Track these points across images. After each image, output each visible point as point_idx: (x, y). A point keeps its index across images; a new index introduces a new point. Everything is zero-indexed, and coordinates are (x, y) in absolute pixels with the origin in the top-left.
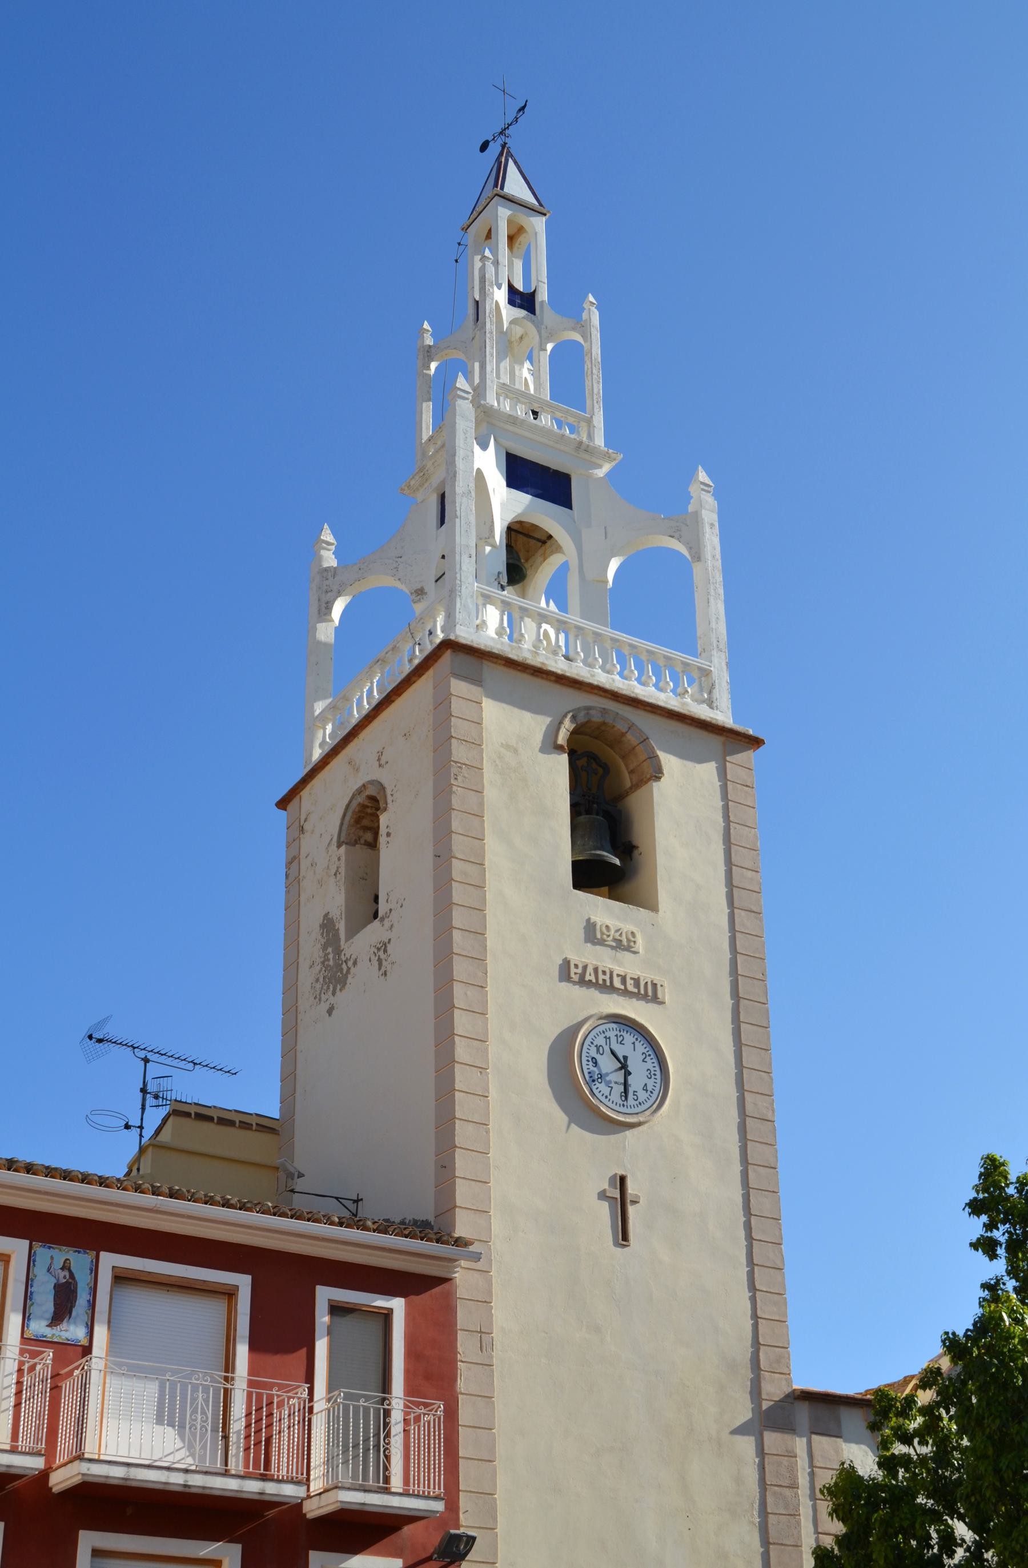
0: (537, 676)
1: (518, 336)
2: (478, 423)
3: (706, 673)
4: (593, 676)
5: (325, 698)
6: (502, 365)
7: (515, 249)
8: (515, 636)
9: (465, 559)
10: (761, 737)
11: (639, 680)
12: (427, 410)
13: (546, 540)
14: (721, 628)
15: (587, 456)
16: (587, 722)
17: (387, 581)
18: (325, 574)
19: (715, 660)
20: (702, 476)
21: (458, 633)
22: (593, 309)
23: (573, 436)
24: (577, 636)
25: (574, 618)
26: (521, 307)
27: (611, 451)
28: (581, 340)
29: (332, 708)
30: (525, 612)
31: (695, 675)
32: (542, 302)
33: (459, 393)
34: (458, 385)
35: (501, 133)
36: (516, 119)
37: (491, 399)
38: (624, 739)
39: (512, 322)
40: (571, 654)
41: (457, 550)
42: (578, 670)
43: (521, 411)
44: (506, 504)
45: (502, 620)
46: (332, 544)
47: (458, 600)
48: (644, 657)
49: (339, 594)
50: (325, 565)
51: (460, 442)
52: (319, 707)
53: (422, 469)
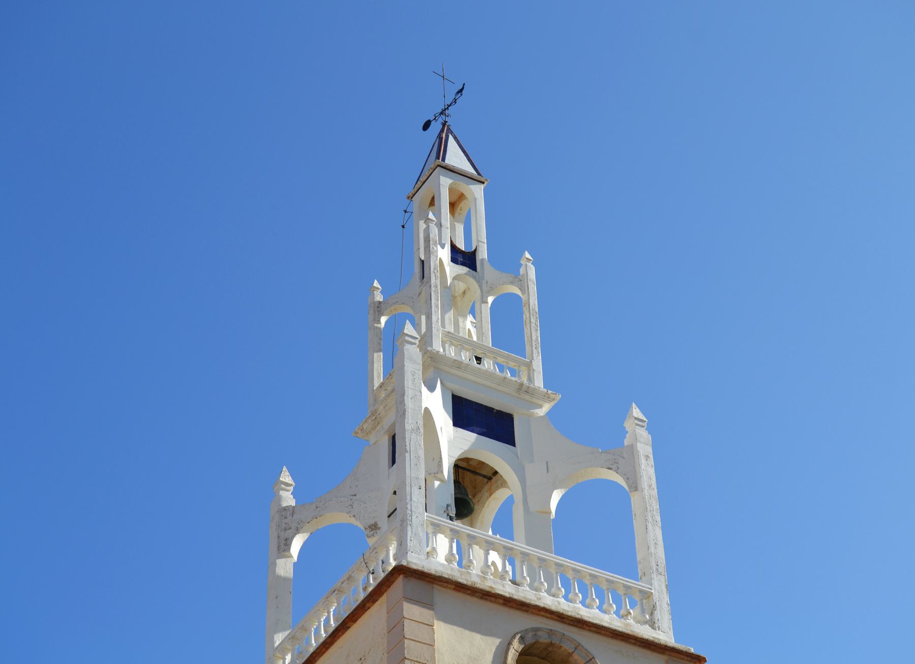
0: (486, 599)
1: (462, 291)
2: (425, 368)
3: (647, 595)
4: (539, 599)
5: (284, 630)
6: (447, 316)
7: (457, 215)
8: (464, 562)
9: (415, 490)
10: (702, 655)
11: (583, 603)
12: (378, 360)
13: (490, 476)
14: (660, 552)
15: (527, 397)
16: (535, 643)
17: (342, 518)
18: (284, 513)
19: (655, 583)
20: (636, 412)
21: (409, 559)
22: (530, 264)
23: (514, 379)
24: (523, 562)
25: (519, 544)
26: (463, 264)
27: (550, 392)
28: (519, 293)
29: (291, 638)
30: (473, 539)
31: (637, 597)
32: (483, 260)
33: (407, 338)
34: (406, 331)
35: (442, 113)
36: (455, 101)
37: (437, 346)
38: (571, 659)
39: (455, 278)
40: (518, 579)
41: (408, 482)
42: (525, 594)
43: (465, 357)
44: (454, 442)
45: (451, 547)
46: (291, 485)
47: (409, 528)
48: (587, 581)
49: (298, 531)
50: (284, 504)
51: (408, 382)
52: (279, 638)
53: (374, 413)
